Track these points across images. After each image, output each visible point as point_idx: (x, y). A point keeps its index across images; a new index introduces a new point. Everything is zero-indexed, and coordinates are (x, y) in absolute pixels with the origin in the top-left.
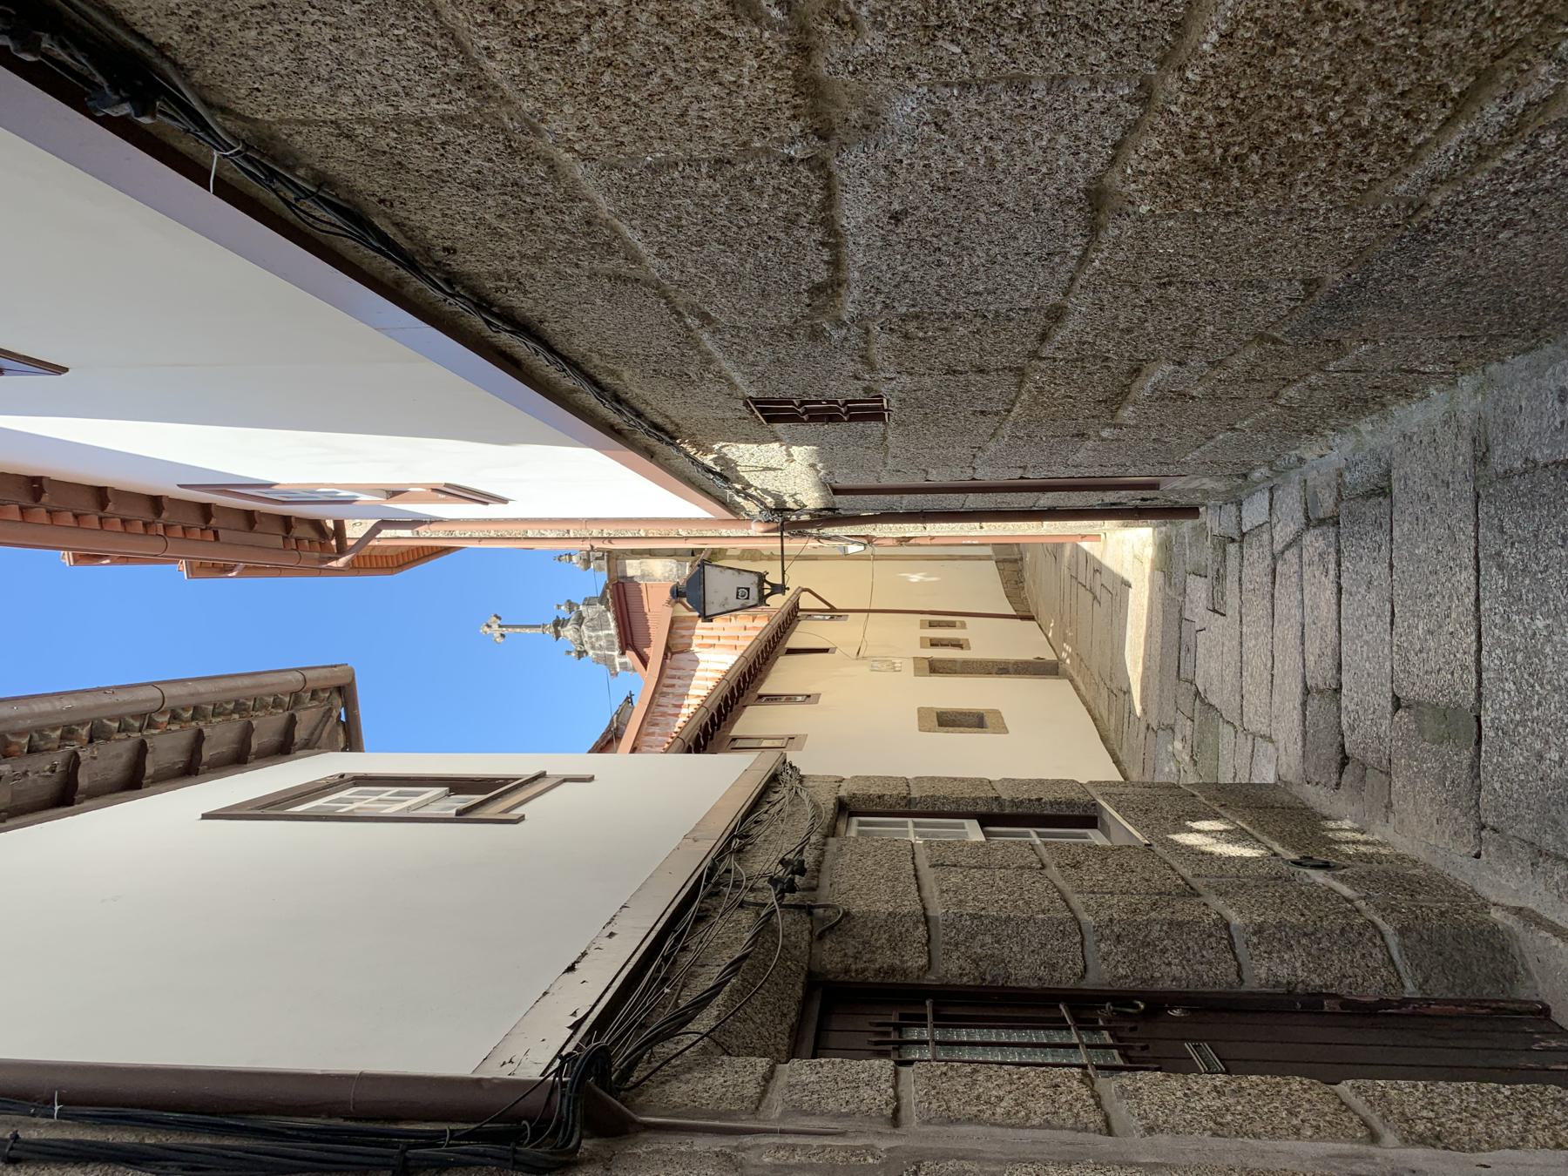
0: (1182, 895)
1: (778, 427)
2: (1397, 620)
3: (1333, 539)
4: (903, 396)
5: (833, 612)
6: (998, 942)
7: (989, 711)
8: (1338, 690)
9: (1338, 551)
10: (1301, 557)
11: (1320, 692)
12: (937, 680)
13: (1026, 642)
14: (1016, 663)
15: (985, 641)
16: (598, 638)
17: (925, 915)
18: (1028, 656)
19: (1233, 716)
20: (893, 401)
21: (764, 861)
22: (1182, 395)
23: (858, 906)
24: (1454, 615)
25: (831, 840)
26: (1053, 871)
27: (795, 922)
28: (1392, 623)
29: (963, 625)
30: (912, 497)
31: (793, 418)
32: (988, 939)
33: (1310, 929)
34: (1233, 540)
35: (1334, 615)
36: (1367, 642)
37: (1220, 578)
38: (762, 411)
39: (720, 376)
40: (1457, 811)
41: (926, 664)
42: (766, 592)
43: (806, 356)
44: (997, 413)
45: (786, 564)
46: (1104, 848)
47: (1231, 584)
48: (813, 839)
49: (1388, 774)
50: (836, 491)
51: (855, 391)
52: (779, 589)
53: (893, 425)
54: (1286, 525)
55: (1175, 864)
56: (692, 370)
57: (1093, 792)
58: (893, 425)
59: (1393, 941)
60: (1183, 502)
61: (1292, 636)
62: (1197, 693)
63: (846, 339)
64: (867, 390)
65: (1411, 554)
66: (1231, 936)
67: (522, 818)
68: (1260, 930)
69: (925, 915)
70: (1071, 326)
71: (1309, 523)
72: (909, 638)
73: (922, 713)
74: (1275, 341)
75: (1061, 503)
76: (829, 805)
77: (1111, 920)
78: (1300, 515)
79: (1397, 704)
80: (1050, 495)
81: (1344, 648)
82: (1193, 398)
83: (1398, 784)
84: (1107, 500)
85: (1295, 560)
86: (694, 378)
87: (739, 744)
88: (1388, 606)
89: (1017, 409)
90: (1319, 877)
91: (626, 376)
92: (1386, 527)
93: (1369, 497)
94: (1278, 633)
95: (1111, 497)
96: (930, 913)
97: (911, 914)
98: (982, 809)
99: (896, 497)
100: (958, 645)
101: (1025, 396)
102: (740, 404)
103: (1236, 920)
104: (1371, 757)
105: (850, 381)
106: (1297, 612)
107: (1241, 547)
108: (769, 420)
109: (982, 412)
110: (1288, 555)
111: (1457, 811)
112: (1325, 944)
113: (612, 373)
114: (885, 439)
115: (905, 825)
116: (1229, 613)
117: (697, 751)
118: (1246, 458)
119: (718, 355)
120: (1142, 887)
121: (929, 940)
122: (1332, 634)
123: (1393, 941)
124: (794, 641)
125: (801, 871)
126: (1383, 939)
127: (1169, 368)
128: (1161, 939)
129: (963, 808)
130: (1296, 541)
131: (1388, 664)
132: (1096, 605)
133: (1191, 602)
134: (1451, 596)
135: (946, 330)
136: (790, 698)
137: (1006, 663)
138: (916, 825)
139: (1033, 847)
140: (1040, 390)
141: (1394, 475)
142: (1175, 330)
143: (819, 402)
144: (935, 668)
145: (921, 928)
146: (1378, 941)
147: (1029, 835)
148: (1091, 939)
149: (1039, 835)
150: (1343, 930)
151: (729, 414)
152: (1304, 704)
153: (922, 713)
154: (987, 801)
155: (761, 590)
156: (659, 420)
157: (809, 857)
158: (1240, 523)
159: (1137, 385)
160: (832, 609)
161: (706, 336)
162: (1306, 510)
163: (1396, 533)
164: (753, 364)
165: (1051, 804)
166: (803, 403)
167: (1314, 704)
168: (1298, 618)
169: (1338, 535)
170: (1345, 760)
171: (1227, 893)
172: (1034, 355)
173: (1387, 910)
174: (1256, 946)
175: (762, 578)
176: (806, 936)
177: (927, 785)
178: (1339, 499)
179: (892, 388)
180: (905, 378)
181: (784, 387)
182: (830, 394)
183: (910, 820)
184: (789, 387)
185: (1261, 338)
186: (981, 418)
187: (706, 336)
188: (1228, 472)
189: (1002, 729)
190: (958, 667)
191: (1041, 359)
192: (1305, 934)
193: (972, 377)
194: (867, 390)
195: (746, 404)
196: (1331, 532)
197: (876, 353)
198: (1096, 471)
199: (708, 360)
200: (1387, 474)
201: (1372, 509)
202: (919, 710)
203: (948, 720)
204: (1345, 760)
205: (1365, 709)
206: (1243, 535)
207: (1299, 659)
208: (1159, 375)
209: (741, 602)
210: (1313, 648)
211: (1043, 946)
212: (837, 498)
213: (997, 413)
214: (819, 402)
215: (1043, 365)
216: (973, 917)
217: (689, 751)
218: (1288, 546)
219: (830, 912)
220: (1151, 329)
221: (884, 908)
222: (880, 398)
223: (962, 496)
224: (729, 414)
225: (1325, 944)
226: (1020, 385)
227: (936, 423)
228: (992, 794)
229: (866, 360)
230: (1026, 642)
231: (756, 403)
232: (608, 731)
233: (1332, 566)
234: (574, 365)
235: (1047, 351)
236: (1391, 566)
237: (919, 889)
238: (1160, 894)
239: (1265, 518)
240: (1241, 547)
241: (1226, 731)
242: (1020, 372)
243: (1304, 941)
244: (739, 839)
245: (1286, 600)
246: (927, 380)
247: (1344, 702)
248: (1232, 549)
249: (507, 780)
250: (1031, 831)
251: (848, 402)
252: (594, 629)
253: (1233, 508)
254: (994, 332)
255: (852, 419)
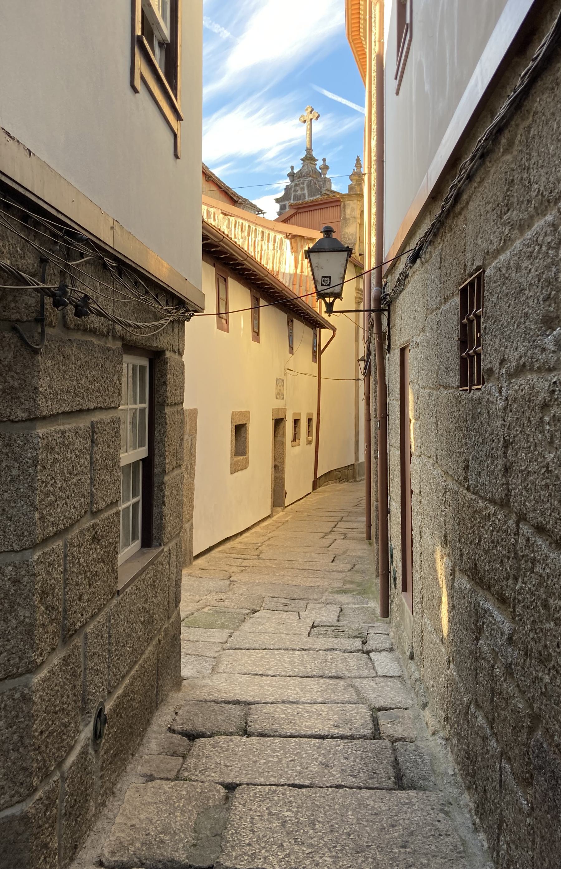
0: (64, 628)
1: (457, 300)
2: (296, 791)
3: (362, 733)
4: (484, 403)
5: (317, 352)
6: (12, 481)
7: (247, 459)
8: (246, 733)
9: (353, 737)
10: (350, 703)
11: (247, 715)
12: (271, 424)
13: (297, 483)
14: (283, 479)
15: (298, 455)
16: (303, 189)
17: (36, 419)
18: (288, 486)
19: (232, 642)
20: (478, 394)
21: (89, 285)
22: (480, 630)
23: (44, 362)
24: (296, 848)
25: (119, 344)
26: (87, 523)
27: (28, 307)
28: (294, 785)
29: (310, 443)
30: (398, 408)
31: (464, 309)
32: (15, 472)
33: (27, 741)
34: (364, 643)
35: (303, 733)
36: (280, 761)
37: (337, 632)
38: (471, 284)
39: (507, 241)
40: (138, 845)
41: (281, 417)
42: (327, 299)
43: (526, 314)
44: (466, 479)
45: (352, 315)
46: (115, 558)
47: (331, 642)
48: (118, 327)
49: (176, 779)
50: (403, 351)
51: (490, 360)
52: (330, 309)
53: (457, 393)
54: (374, 690)
55: (99, 618)
56: (514, 215)
57: (172, 544)
58: (457, 393)
59: (16, 810)
60: (393, 607)
61: (290, 694)
62: (254, 612)
63: (544, 350)
64: (490, 371)
65: (347, 808)
66: (21, 675)
67: (136, 91)
68: (26, 699)
69: (36, 419)
70: (552, 555)
71: (376, 711)
72: (300, 405)
73: (246, 414)
74: (532, 730)
75: (393, 518)
76: (157, 344)
77: (34, 575)
78: (381, 703)
79: (231, 787)
80: (399, 510)
81: (278, 740)
82: (477, 639)
83: (167, 786)
84: (395, 551)
85: (347, 697)
86: (505, 217)
87: (221, 280)
88: (307, 782)
89: (470, 496)
90: (87, 732)
91: (509, 157)
92: (371, 783)
93: (394, 767)
94: (293, 681)
95: (397, 555)
96: (38, 424)
97: (37, 406)
98: (157, 460)
99: (398, 396)
100: (295, 437)
101: (481, 504)
102: (477, 263)
103: (36, 679)
104: (191, 762)
105: (499, 357)
106: (307, 698)
107: (358, 651)
108: (463, 292)
109: (467, 467)
110: (351, 691)
111: (138, 845)
112: (13, 755)
113: (511, 144)
114: (445, 387)
115: (142, 401)
116: (310, 640)
117: (204, 246)
118: (427, 663)
119: (528, 234)
120: (70, 596)
121: (13, 421)
122: (290, 730)
123: (16, 810)
124: (297, 324)
125: (79, 313)
126: (18, 802)
127: (506, 627)
128: (16, 617)
129: (157, 446)
130: (361, 699)
131: (262, 780)
132: (322, 535)
133: (320, 608)
134: (312, 846)
135: (551, 443)
136: (291, 336)
137: (283, 472)
138: (142, 411)
139: (114, 503)
140: (487, 517)
141: (412, 793)
142: (546, 646)
143: (479, 330)
144: (278, 422)
145: (25, 415)
146: (16, 799)
147: (134, 496)
148: (17, 558)
149: (135, 505)
150: (25, 769)
151: (469, 255)
152: (237, 702)
153: (246, 414)
154: (163, 464)
155: (329, 295)
156: (465, 197)
157: (94, 321)
158: (377, 651)
159: (490, 597)
160: (321, 352)
161: (549, 218)
162: (385, 709)
163: (365, 793)
164: (518, 268)
165: (161, 512)
166: (478, 317)
167: (237, 711)
168: (303, 699)
169: (364, 737)
170: (192, 736)
171: (67, 664)
172: (522, 518)
173: (49, 802)
174: (12, 697)
175: (338, 295)
176: (15, 317)
177: (177, 418)
178: (394, 741)
179: (492, 392)
180: (501, 404)
181: (494, 299)
182: (487, 339)
183: (146, 405)
184: (493, 302)
185: (536, 718)
186: (461, 465)
187: (549, 218)
188: (415, 645)
189: (235, 469)
190: (279, 438)
191: (517, 523)
192: (22, 737)
193: (500, 463)
194: (490, 371)
195: (478, 268)
196: (368, 731)
197: (523, 382)
198: (417, 549)
199: (523, 226)
200: (412, 787)
201: (386, 772)
202: (248, 412)
203: (240, 430)
204: (192, 736)
205: (224, 758)
206: (368, 653)
207: (272, 699)
208: (500, 618)
209: (320, 280)
210: (279, 711)
211: (9, 519)
212: (397, 352)
213: (466, 479)
214: (479, 330)
215: (511, 523)
216: (35, 460)
217: (205, 238)
218: (357, 691)
219: (37, 337)
220: (547, 626)
221: (43, 384)
222: (481, 381)
223: (398, 445)
224: (469, 255)
225: (13, 755)
226: (492, 501)
227: (458, 428)
228: (168, 468)
229: (521, 370)
230: (297, 483)
231: (479, 277)
232: (239, 197)
233: (341, 732)
234: (519, 104)
235: (525, 529)
236: (338, 787)
237: (65, 413)
238: (65, 611)
239: (380, 672)
240: (358, 651)
241: (225, 634)
242: (504, 503)
243: (15, 737)
244: (123, 270)
245: (315, 689)
246: (499, 423)
247: (236, 738)
248: (358, 644)
249: (175, 89)
250: (139, 498)
251: (479, 355)
252: (309, 186)
253: (388, 646)
254: (547, 486)
255: (463, 361)
